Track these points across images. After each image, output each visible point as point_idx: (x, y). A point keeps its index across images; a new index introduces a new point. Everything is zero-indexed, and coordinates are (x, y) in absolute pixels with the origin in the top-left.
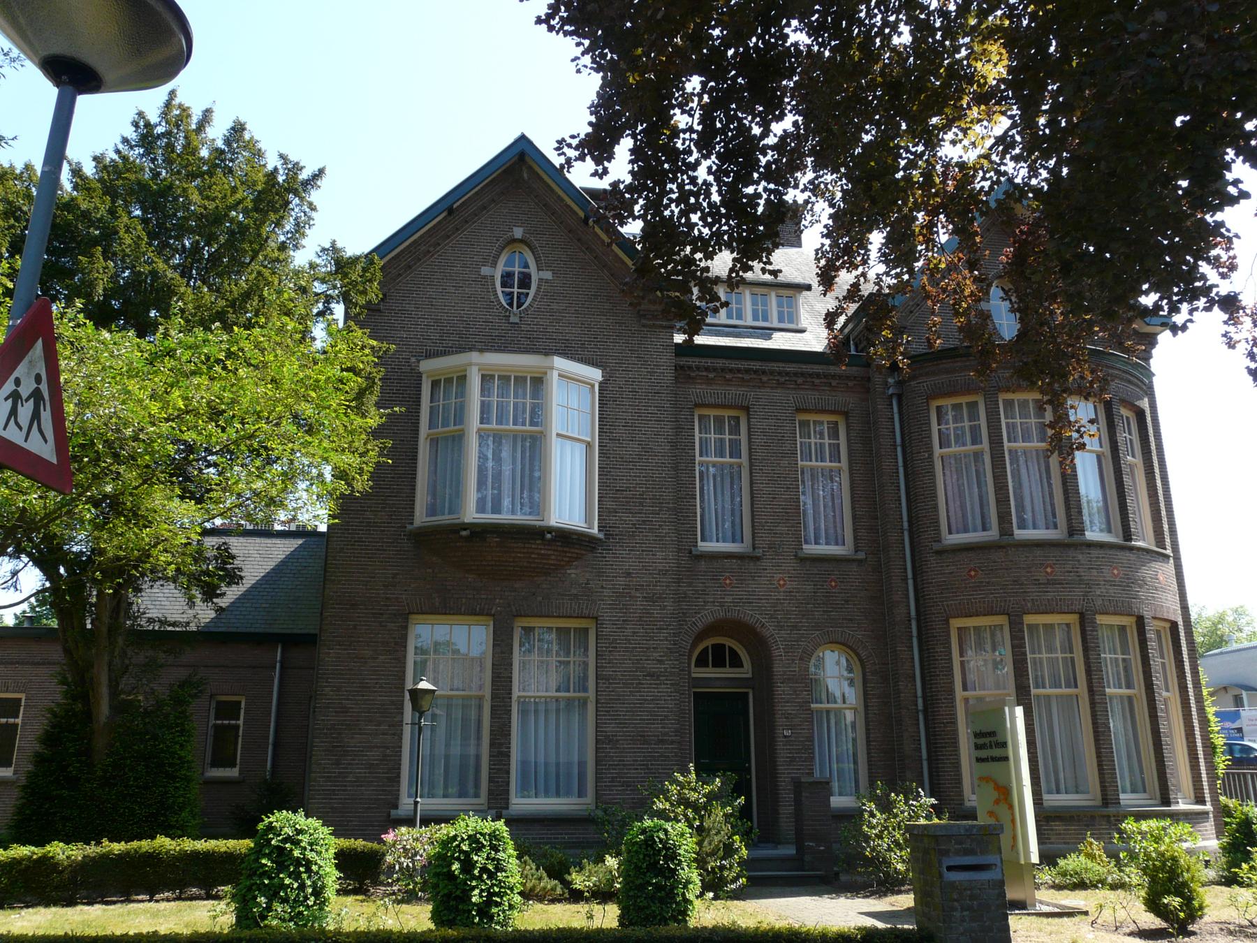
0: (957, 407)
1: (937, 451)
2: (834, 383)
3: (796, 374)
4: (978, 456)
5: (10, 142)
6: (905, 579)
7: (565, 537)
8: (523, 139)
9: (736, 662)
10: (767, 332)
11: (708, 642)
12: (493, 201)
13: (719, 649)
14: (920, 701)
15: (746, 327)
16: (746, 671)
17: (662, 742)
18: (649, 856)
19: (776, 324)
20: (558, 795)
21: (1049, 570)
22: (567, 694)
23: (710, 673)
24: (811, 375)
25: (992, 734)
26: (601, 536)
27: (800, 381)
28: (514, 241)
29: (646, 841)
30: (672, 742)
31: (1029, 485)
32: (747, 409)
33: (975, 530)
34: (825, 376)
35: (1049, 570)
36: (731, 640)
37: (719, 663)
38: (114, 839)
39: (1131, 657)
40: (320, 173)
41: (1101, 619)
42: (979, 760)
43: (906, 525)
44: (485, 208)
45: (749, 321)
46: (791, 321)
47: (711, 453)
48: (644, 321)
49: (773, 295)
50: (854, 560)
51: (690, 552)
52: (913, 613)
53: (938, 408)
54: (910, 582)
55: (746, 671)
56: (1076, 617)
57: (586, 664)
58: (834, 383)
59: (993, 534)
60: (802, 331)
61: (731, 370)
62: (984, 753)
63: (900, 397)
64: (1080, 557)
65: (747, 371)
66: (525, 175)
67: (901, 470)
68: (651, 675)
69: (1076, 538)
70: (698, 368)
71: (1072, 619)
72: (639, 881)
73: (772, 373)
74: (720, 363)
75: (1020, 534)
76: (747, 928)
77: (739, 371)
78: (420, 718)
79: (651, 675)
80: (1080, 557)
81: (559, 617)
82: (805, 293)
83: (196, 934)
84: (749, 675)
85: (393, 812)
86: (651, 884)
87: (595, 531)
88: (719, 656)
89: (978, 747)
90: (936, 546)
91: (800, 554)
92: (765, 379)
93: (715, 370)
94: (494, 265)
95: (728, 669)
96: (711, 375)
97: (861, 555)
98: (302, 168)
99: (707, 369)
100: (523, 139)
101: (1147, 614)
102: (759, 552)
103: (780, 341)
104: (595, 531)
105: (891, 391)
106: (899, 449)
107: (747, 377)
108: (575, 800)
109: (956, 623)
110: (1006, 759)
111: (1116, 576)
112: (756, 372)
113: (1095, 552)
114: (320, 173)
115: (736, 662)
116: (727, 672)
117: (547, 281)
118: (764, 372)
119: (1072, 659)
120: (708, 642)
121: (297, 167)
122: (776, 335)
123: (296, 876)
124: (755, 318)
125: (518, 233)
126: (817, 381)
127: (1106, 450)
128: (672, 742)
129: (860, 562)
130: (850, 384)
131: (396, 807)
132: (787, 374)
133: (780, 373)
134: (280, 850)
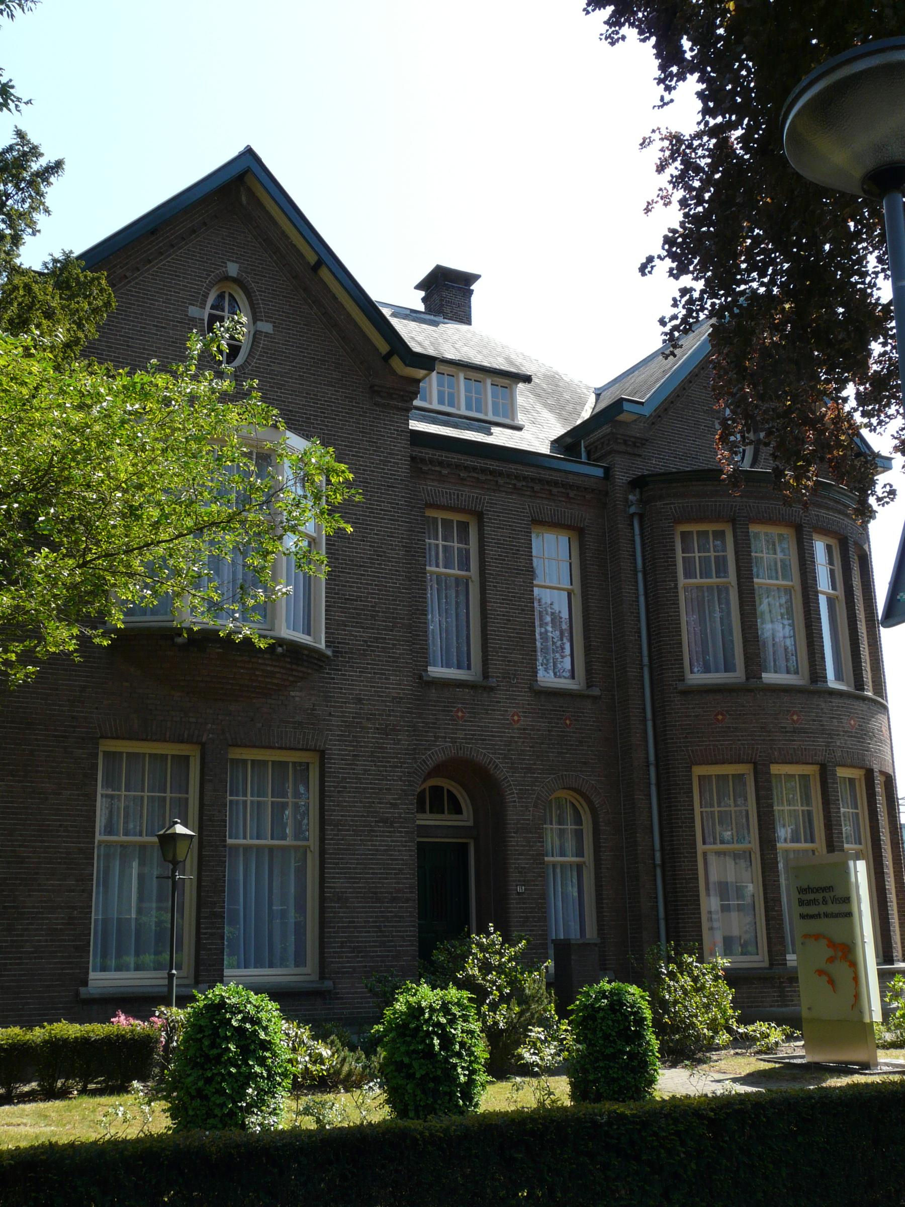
0: (703, 534)
1: (682, 581)
2: (572, 494)
3: (533, 480)
4: (722, 590)
5: (22, 106)
6: (645, 720)
7: (293, 653)
8: (249, 153)
9: (457, 809)
10: (485, 426)
11: (433, 782)
12: (205, 224)
13: (436, 791)
14: (658, 855)
15: (461, 417)
16: (466, 819)
17: (394, 900)
18: (618, 1022)
19: (490, 417)
20: (271, 966)
21: (795, 717)
22: (137, 839)
23: (428, 820)
24: (549, 483)
25: (830, 889)
26: (329, 653)
27: (537, 487)
28: (227, 278)
29: (611, 1005)
30: (407, 900)
31: (778, 629)
32: (480, 516)
33: (717, 671)
34: (564, 485)
35: (795, 717)
36: (461, 784)
37: (436, 808)
38: (72, 1021)
39: (859, 811)
40: (58, 166)
41: (843, 773)
42: (803, 916)
43: (646, 660)
44: (194, 231)
45: (463, 411)
46: (505, 416)
47: (445, 562)
48: (379, 399)
49: (461, 376)
50: (588, 697)
51: (421, 677)
52: (652, 758)
53: (683, 534)
54: (650, 724)
55: (466, 819)
56: (816, 768)
57: (809, 815)
58: (572, 494)
59: (738, 675)
60: (519, 428)
61: (466, 468)
62: (813, 910)
63: (641, 517)
64: (823, 705)
65: (483, 471)
66: (244, 199)
67: (642, 599)
68: (384, 821)
69: (820, 685)
70: (431, 462)
71: (810, 770)
72: (609, 1051)
73: (509, 476)
74: (455, 458)
75: (769, 677)
76: (688, 1097)
77: (475, 469)
78: (174, 871)
79: (384, 821)
80: (823, 705)
81: (280, 748)
82: (521, 386)
83: (519, 1112)
84: (470, 823)
85: (82, 990)
86: (625, 1053)
87: (322, 646)
88: (435, 800)
89: (801, 903)
90: (681, 687)
91: (536, 688)
92: (501, 481)
93: (449, 465)
94: (203, 306)
95: (446, 816)
96: (445, 472)
97: (596, 692)
98: (41, 155)
99: (441, 464)
100: (249, 153)
101: (876, 768)
102: (493, 682)
103: (500, 437)
104: (322, 646)
105: (633, 510)
106: (640, 575)
107: (482, 477)
108: (292, 970)
109: (698, 771)
110: (849, 914)
111: (853, 727)
112: (492, 472)
113: (836, 701)
114: (58, 166)
115: (457, 809)
116: (446, 820)
117: (267, 335)
118: (501, 474)
119: (809, 813)
120: (433, 782)
121: (35, 152)
122: (495, 430)
123: (262, 1062)
124: (469, 407)
125: (233, 269)
126: (555, 490)
127: (840, 593)
128: (407, 900)
129: (595, 698)
130: (588, 497)
131: (85, 984)
132: (525, 478)
133: (517, 477)
134: (240, 1030)
